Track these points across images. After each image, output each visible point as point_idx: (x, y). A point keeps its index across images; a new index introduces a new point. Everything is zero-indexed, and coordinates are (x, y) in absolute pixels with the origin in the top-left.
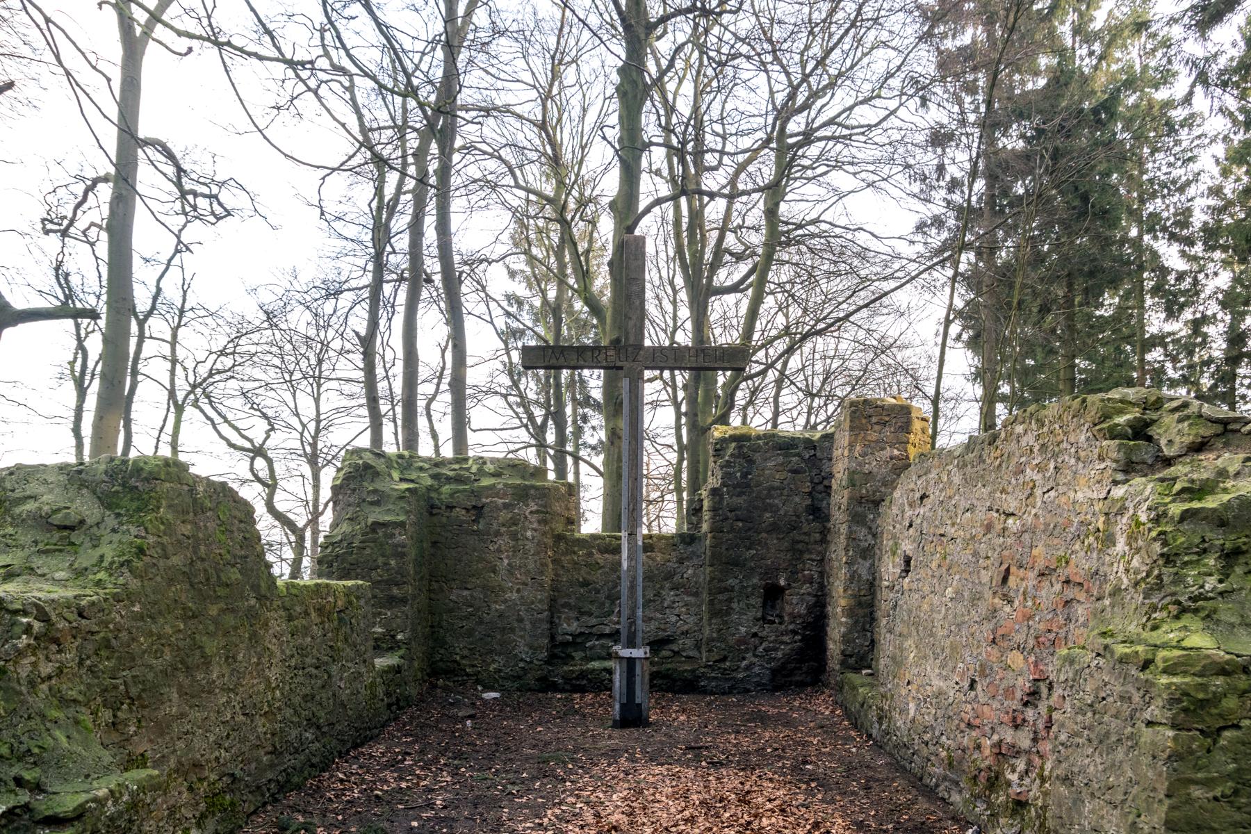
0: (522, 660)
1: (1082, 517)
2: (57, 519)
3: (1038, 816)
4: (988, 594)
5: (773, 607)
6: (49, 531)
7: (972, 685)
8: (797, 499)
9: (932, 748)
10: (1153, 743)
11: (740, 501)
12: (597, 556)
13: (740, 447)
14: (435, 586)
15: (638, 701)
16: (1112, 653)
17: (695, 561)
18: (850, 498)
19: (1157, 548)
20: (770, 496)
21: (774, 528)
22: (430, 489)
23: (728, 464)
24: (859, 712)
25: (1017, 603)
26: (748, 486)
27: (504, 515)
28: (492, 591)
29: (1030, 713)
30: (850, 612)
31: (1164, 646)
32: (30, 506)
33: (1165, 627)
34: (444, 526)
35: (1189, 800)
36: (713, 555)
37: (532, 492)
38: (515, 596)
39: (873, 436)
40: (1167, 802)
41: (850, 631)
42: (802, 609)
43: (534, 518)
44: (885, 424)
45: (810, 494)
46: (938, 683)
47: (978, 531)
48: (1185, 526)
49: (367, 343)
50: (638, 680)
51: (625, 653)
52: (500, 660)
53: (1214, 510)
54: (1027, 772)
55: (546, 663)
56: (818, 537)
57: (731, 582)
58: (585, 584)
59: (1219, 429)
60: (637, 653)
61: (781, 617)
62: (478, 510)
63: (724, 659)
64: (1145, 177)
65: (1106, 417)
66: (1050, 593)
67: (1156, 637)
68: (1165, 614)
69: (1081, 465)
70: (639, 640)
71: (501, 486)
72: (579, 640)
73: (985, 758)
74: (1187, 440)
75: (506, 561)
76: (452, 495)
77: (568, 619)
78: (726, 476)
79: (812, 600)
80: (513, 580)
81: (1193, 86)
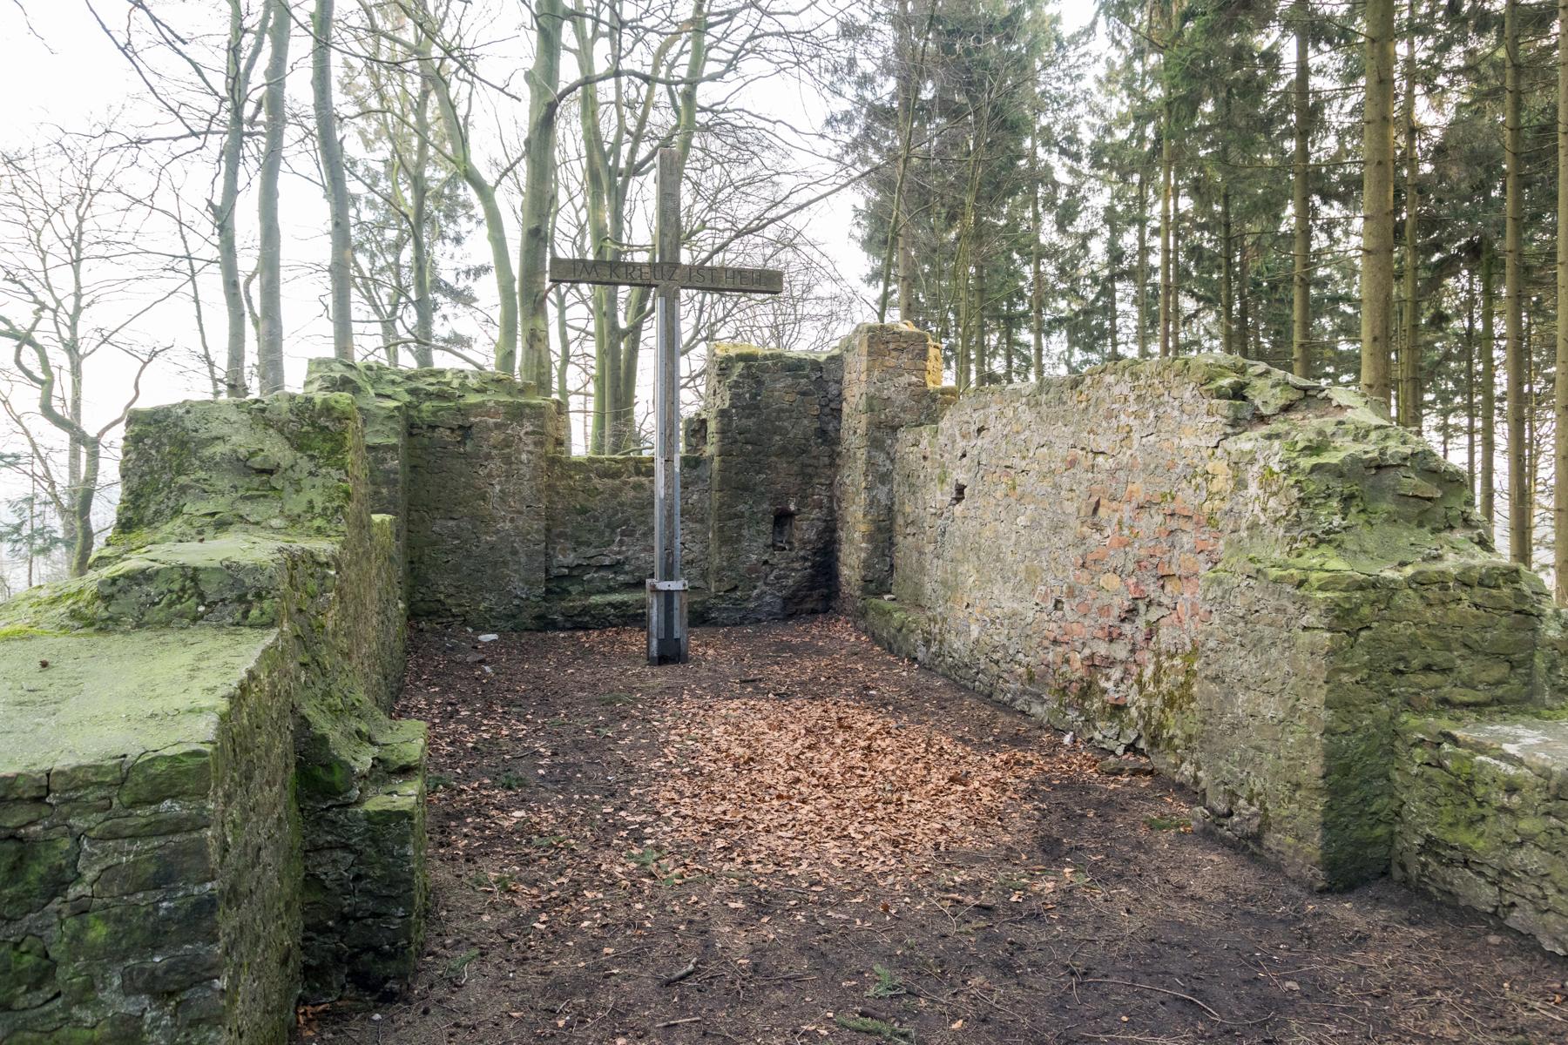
0: (516, 597)
1: (1188, 461)
2: (257, 462)
3: (1142, 716)
4: (1074, 523)
5: (781, 533)
6: (247, 475)
7: (1058, 604)
8: (806, 422)
9: (1004, 666)
10: (1312, 643)
11: (750, 422)
12: (596, 481)
13: (749, 367)
14: (415, 515)
15: (677, 636)
16: (1265, 575)
17: (701, 486)
18: (869, 423)
19: (1295, 493)
20: (779, 418)
21: (783, 451)
22: (409, 405)
23: (736, 384)
24: (895, 637)
25: (1108, 531)
26: (757, 407)
27: (496, 437)
28: (485, 521)
29: (1127, 628)
30: (870, 538)
31: (1311, 569)
32: (220, 448)
33: (1307, 555)
34: (425, 448)
35: (1341, 685)
36: (724, 481)
37: (527, 411)
38: (508, 525)
39: (890, 362)
40: (1326, 687)
41: (870, 557)
42: (812, 535)
43: (529, 440)
44: (902, 350)
45: (818, 417)
46: (1009, 605)
47: (1059, 465)
48: (1314, 477)
49: (223, 217)
50: (676, 613)
51: (664, 586)
52: (493, 597)
53: (1336, 465)
54: (1122, 680)
55: (545, 599)
56: (826, 460)
57: (741, 507)
58: (583, 511)
59: (1301, 394)
60: (675, 585)
61: (790, 543)
62: (465, 430)
63: (735, 588)
64: (1037, 90)
65: (1211, 379)
66: (1152, 522)
67: (1301, 562)
68: (1305, 544)
69: (1185, 417)
70: (677, 572)
71: (491, 404)
72: (575, 573)
73: (1077, 669)
74: (1281, 402)
75: (498, 488)
76: (434, 413)
77: (564, 549)
78: (735, 397)
79: (822, 525)
80: (508, 510)
81: (1097, 14)
